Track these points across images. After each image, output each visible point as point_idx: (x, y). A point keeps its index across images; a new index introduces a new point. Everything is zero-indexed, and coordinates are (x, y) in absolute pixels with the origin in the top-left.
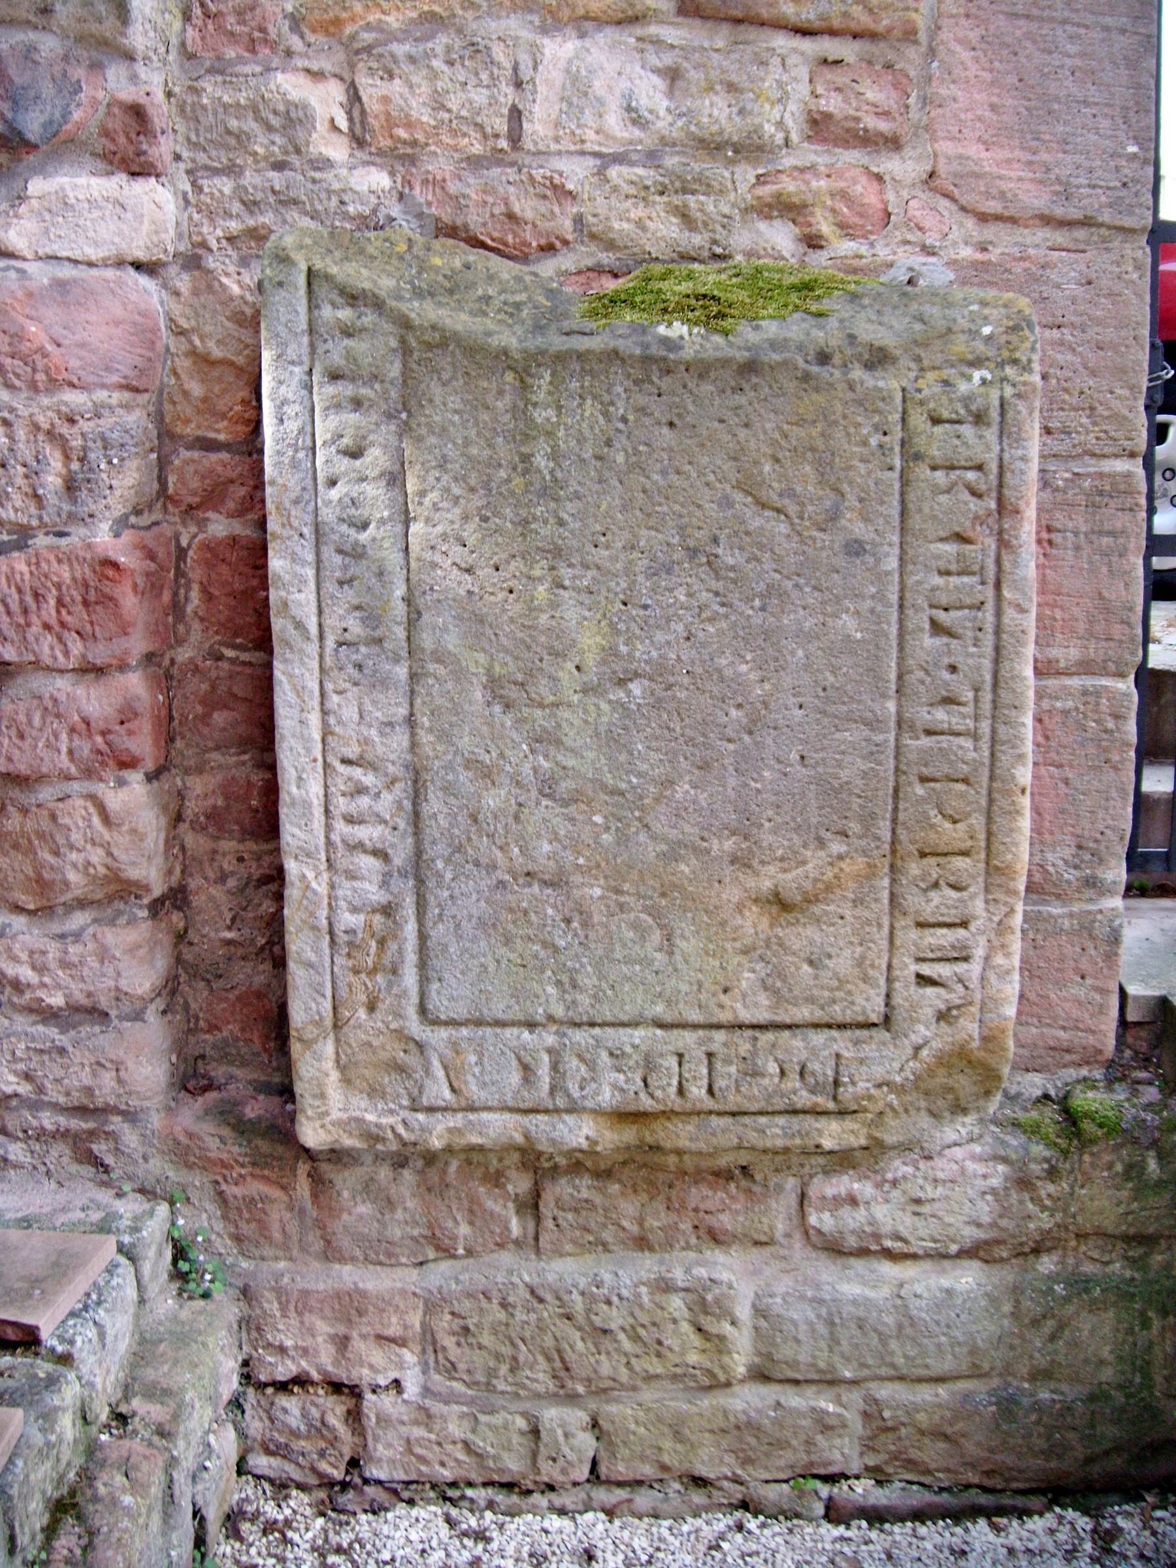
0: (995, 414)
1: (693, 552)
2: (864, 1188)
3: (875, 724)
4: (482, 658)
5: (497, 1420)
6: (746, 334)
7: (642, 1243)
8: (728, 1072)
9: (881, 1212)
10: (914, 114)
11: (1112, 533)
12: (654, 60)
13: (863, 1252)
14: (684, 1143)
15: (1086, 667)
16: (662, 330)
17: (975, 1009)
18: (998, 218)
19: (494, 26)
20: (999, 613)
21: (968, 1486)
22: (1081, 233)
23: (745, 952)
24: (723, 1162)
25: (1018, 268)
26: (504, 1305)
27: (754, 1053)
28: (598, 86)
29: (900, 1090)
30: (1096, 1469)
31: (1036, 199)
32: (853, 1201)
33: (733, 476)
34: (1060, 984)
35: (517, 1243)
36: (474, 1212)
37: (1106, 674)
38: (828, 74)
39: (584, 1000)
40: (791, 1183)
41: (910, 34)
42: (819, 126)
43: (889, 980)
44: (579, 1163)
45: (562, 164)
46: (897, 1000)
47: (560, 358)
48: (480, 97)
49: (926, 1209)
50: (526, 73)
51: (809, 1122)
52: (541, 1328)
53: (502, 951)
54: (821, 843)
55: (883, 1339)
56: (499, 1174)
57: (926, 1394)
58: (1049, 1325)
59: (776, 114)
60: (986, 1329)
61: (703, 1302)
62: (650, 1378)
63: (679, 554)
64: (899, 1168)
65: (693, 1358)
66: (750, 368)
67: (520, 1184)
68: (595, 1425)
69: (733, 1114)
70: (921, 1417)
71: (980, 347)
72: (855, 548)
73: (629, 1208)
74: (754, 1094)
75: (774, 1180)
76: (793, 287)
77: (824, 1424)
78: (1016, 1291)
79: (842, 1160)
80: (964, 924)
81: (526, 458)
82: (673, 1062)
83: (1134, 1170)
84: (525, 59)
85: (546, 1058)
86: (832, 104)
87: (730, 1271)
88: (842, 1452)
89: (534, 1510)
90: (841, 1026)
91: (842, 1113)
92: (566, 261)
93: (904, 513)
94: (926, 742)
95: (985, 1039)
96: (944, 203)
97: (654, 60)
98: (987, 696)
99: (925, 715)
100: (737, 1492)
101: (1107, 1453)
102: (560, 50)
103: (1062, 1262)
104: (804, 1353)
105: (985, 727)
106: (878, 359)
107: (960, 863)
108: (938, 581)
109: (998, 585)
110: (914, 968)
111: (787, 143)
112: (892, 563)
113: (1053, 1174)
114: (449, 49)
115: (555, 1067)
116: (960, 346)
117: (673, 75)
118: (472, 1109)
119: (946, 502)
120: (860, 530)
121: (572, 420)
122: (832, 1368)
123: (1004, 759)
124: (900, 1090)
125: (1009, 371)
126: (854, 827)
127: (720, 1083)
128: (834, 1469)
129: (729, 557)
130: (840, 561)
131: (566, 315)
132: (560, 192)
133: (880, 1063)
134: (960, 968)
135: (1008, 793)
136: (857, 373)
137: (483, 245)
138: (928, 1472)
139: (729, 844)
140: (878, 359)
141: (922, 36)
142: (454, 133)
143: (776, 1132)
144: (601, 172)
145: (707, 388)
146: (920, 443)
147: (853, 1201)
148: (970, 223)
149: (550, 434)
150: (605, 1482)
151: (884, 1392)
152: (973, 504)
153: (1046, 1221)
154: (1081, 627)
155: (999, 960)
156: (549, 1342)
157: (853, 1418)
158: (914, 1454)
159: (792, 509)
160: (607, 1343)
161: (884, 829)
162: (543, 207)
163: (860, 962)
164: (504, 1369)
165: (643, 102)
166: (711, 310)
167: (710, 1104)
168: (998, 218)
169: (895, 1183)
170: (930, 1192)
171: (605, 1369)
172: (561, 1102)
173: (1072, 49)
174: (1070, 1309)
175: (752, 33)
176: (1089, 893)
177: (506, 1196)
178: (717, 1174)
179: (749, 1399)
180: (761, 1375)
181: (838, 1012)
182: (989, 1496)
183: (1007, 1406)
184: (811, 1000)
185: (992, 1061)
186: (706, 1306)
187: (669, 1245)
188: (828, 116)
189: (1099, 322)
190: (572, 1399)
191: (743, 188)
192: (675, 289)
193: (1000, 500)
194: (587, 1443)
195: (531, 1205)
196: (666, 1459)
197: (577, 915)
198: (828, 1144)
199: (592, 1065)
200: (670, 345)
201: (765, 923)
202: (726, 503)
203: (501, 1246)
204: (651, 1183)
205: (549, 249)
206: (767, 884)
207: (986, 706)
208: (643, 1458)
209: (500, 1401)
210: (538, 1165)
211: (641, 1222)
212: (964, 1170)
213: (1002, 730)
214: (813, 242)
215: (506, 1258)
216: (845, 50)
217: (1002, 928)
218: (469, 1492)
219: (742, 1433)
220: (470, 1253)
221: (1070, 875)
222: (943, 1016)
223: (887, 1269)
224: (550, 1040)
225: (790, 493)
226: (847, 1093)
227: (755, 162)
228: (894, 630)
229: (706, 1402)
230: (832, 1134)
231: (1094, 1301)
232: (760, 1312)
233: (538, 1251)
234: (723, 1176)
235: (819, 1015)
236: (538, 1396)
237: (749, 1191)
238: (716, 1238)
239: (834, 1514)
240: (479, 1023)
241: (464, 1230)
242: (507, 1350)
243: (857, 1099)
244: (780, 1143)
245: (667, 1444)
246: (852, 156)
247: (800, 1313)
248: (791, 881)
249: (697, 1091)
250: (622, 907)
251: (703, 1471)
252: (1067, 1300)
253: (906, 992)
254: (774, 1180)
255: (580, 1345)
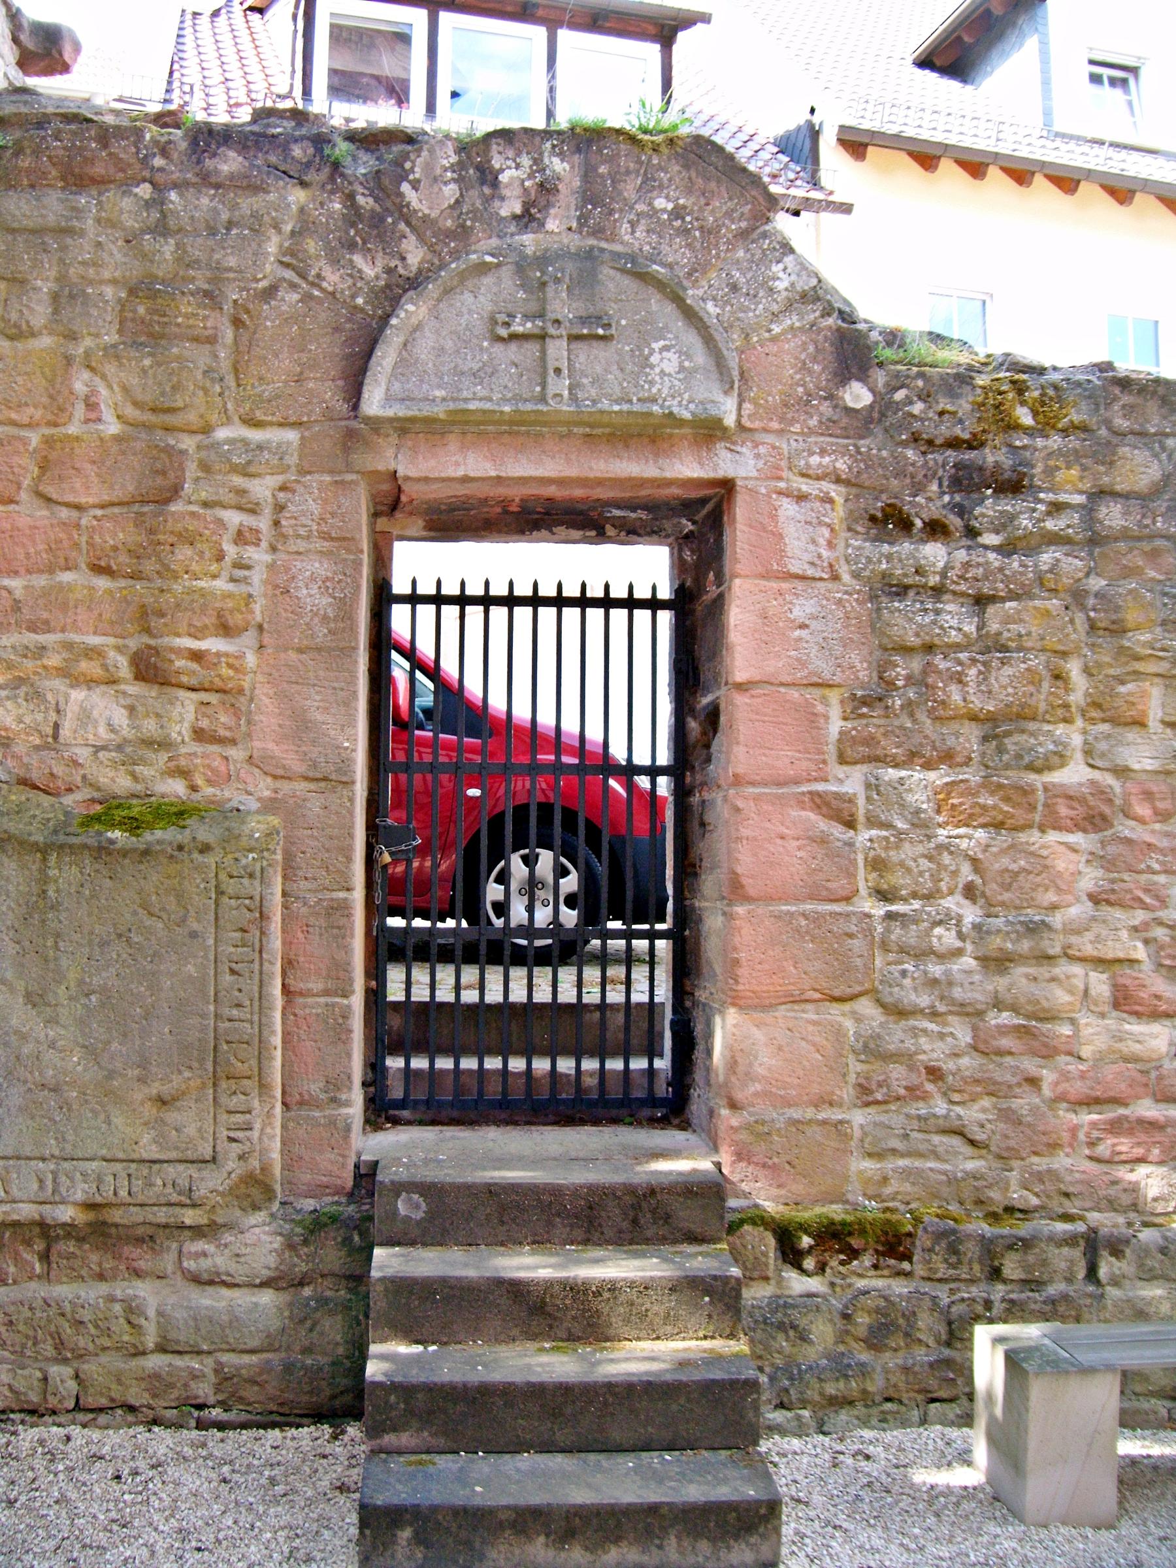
0: (258, 874)
1: (120, 936)
2: (210, 1248)
3: (204, 1016)
4: (22, 983)
5: (26, 1372)
6: (148, 836)
7: (101, 1277)
8: (138, 1184)
9: (219, 1260)
10: (243, 728)
11: (339, 928)
12: (122, 702)
13: (211, 1283)
14: (117, 1220)
15: (327, 993)
16: (109, 834)
17: (256, 1154)
18: (282, 777)
19: (47, 683)
20: (261, 965)
21: (271, 1413)
22: (323, 784)
23: (145, 1124)
24: (140, 1231)
25: (291, 801)
26: (31, 1309)
27: (150, 1174)
28: (95, 713)
29: (222, 1194)
30: (337, 1403)
31: (299, 768)
32: (205, 1254)
33: (138, 901)
34: (321, 1152)
35: (39, 1277)
36: (17, 1258)
37: (337, 995)
38: (203, 709)
39: (69, 1147)
40: (175, 1245)
41: (241, 691)
42: (199, 735)
43: (215, 1139)
44: (69, 1230)
45: (77, 750)
46: (218, 1149)
47: (61, 847)
48: (39, 717)
49: (242, 1260)
50: (62, 706)
51: (177, 1210)
52: (49, 1321)
53: (29, 1122)
54: (180, 1072)
55: (223, 1329)
56: (30, 1239)
57: (246, 1359)
58: (308, 1323)
59: (177, 728)
60: (275, 1324)
61: (130, 1307)
62: (104, 1349)
63: (113, 937)
64: (228, 1237)
65: (126, 1338)
66: (146, 853)
67: (39, 1246)
68: (77, 1376)
69: (141, 1205)
70: (244, 1372)
71: (253, 843)
72: (194, 935)
73: (94, 1257)
74: (150, 1195)
75: (166, 1244)
76: (175, 814)
77: (195, 1376)
78: (290, 1305)
79: (198, 1232)
80: (249, 1112)
81: (44, 892)
82: (111, 1178)
83: (347, 1241)
84: (62, 700)
85: (50, 1176)
86: (204, 723)
87: (144, 1291)
88: (204, 1390)
89: (45, 1425)
90: (192, 1162)
91: (194, 1206)
92: (78, 796)
93: (217, 919)
94: (227, 1024)
95: (262, 1169)
96: (256, 770)
97: (122, 702)
98: (256, 1004)
99: (227, 1012)
100: (151, 1414)
101: (342, 1393)
102: (78, 695)
103: (315, 1290)
104: (183, 1336)
105: (256, 1018)
106: (205, 849)
107: (245, 1082)
108: (232, 949)
109: (261, 952)
110: (225, 1133)
111: (183, 742)
112: (211, 942)
113: (306, 1242)
114: (27, 694)
115: (54, 1180)
116: (244, 842)
117: (131, 709)
118: (15, 1202)
119: (234, 913)
120: (195, 926)
121: (65, 875)
122: (197, 1344)
123: (265, 1033)
124: (222, 1194)
125: (265, 854)
126: (195, 1065)
127: (134, 1189)
128: (199, 1401)
129: (136, 939)
130: (187, 940)
131: (70, 825)
132: (76, 764)
133: (210, 1183)
134: (248, 1133)
135: (268, 1049)
136: (196, 855)
137: (38, 788)
138: (249, 1404)
139: (136, 1072)
140: (205, 849)
141: (247, 692)
142: (27, 734)
143: (161, 1215)
144: (96, 752)
145: (127, 861)
146: (223, 887)
147: (205, 1254)
148: (269, 780)
149: (56, 881)
150: (85, 1410)
151: (225, 1358)
152: (248, 915)
153: (303, 1267)
154: (324, 973)
155: (268, 1130)
156: (53, 1328)
157: (208, 1371)
158: (242, 1393)
159: (165, 917)
160: (81, 1327)
161: (209, 1066)
162: (67, 770)
163: (200, 1130)
164: (30, 1343)
165: (116, 722)
166: (134, 825)
167: (129, 1200)
168: (282, 777)
169: (226, 1246)
170: (244, 1251)
171: (82, 1344)
172: (57, 1199)
173: (318, 698)
174: (318, 1315)
175: (169, 689)
176: (333, 1105)
177: (33, 1252)
178: (137, 1240)
179: (156, 1362)
180: (162, 1349)
181: (190, 1155)
182: (281, 1417)
183: (288, 1368)
184: (177, 1148)
185: (268, 1181)
186: (132, 1311)
187: (114, 1278)
188: (202, 729)
189: (330, 826)
190: (65, 1361)
191: (161, 763)
192: (118, 814)
193: (261, 913)
194: (72, 1385)
195: (45, 1257)
196: (113, 1394)
197: (65, 1106)
198: (188, 1222)
199: (72, 1179)
200: (112, 842)
201: (154, 1111)
202: (135, 913)
203: (31, 1278)
204: (105, 1244)
205: (70, 790)
206: (155, 1091)
207: (256, 1008)
208: (101, 1394)
209: (28, 1362)
210: (44, 1228)
211: (100, 1265)
212: (260, 1241)
213: (264, 1020)
214: (194, 788)
215: (33, 1285)
216: (213, 698)
217: (269, 1114)
218: (12, 1416)
219: (156, 1382)
220: (15, 1282)
221: (323, 1096)
222: (241, 1157)
223: (224, 1292)
224: (52, 1167)
225: (163, 909)
226: (195, 1195)
227: (168, 751)
228: (212, 973)
229: (134, 1363)
230: (190, 1217)
231: (330, 1310)
232: (160, 1313)
233: (49, 1281)
234: (140, 1241)
235: (180, 1156)
236: (47, 1359)
237: (152, 1249)
238: (138, 1274)
239: (201, 1425)
240: (18, 1158)
241: (12, 1269)
242: (31, 1333)
243: (201, 1198)
244: (164, 1220)
245: (113, 1386)
246: (214, 748)
247: (180, 1315)
248: (166, 1090)
249: (123, 1193)
250: (86, 1101)
251: (133, 1401)
252: (316, 1309)
253: (223, 1145)
254: (166, 1244)
255: (69, 1331)
